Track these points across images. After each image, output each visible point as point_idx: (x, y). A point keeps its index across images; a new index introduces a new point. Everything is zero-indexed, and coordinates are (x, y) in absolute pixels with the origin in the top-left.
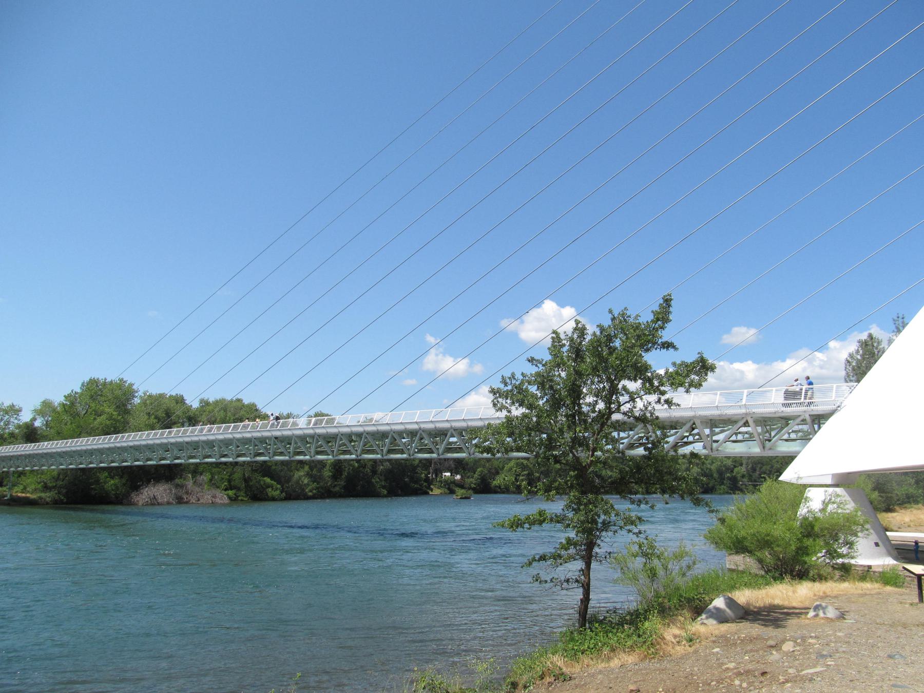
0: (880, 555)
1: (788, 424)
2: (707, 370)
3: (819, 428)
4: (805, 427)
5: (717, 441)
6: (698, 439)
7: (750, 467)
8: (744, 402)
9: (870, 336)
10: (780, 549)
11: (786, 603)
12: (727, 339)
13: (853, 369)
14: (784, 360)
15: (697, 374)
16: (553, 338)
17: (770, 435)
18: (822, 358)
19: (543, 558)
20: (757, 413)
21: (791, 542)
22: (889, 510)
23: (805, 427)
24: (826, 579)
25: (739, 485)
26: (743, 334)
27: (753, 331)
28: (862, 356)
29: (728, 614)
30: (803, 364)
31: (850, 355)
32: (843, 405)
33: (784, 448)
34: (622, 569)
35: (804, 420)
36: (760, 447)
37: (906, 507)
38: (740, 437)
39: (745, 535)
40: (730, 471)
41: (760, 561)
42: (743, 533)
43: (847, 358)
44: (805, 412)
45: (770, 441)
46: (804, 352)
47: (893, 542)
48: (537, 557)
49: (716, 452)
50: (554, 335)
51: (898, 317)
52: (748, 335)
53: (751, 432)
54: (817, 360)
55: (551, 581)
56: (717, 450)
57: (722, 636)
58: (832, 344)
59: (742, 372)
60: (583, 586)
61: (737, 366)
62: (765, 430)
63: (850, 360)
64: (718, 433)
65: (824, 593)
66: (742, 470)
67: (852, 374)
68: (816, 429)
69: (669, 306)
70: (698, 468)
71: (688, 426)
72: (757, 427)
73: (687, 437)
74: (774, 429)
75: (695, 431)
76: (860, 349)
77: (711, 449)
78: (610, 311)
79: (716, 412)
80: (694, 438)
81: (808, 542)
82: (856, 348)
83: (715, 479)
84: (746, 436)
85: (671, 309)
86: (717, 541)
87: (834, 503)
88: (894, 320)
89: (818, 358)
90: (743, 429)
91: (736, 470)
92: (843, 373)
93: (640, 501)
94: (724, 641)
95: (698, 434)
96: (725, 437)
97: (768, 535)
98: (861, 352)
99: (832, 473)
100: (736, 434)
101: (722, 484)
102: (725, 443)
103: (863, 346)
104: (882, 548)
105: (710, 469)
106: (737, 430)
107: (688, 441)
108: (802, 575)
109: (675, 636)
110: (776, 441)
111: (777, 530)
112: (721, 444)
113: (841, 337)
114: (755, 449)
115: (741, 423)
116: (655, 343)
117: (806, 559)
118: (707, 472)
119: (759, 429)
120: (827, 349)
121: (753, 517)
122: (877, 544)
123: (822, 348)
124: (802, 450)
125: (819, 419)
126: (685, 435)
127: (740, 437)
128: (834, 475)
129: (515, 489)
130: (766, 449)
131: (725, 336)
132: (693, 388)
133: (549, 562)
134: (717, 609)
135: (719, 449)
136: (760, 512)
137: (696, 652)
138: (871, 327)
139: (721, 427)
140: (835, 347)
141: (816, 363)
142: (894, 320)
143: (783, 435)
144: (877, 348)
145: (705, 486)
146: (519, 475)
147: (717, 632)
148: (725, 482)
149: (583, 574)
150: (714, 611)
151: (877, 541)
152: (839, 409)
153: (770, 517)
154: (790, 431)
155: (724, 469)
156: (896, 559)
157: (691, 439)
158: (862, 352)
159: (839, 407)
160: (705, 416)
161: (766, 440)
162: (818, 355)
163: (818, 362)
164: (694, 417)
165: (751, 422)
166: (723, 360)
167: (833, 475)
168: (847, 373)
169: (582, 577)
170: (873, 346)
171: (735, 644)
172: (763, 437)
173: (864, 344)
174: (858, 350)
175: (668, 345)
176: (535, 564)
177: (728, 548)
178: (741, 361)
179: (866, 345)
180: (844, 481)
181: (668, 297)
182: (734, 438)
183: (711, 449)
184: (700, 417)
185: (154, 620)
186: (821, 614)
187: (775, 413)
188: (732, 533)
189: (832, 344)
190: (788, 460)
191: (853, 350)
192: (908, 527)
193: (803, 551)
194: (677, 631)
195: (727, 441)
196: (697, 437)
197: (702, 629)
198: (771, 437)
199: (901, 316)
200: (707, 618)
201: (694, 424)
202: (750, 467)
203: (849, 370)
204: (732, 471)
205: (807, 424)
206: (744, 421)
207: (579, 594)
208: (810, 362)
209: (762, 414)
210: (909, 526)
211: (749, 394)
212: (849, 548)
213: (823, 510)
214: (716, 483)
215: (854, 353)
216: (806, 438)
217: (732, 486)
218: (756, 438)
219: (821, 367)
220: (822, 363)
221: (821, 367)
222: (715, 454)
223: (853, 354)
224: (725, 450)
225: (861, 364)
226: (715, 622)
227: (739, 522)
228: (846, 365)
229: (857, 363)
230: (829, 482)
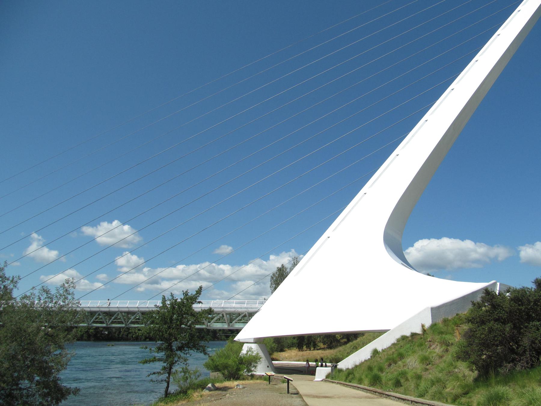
0: (269, 371)
10: (230, 369)
11: (230, 386)
12: (218, 251)
16: (163, 298)
19: (154, 373)
21: (234, 366)
22: (282, 350)
24: (245, 380)
25: (217, 336)
26: (226, 249)
28: (278, 275)
29: (474, 256)
32: (260, 309)
33: (237, 326)
34: (174, 378)
37: (291, 349)
39: (219, 364)
41: (223, 374)
42: (218, 363)
44: (246, 311)
47: (274, 366)
48: (152, 373)
50: (163, 297)
55: (156, 381)
56: (210, 326)
57: (210, 395)
58: (272, 257)
59: (223, 271)
60: (167, 382)
61: (222, 266)
65: (243, 383)
69: (201, 290)
76: (278, 272)
77: (207, 326)
78: (183, 291)
81: (241, 366)
82: (276, 271)
83: (205, 332)
86: (207, 366)
87: (251, 351)
93: (187, 353)
94: (211, 396)
97: (227, 364)
98: (278, 273)
101: (208, 334)
104: (270, 368)
108: (237, 379)
109: (197, 395)
111: (230, 362)
114: (225, 326)
116: (196, 301)
117: (239, 372)
121: (222, 357)
122: (268, 367)
129: (86, 338)
133: (156, 375)
134: (209, 387)
136: (224, 355)
137: (203, 399)
144: (285, 272)
146: (90, 329)
147: (209, 394)
148: (210, 334)
149: (167, 378)
150: (208, 388)
151: (269, 365)
153: (228, 357)
156: (274, 372)
159: (259, 310)
167: (254, 338)
168: (271, 283)
169: (167, 380)
170: (283, 271)
171: (214, 396)
175: (200, 302)
176: (151, 375)
177: (212, 369)
178: (225, 264)
179: (280, 270)
180: (259, 341)
183: (207, 326)
186: (238, 387)
187: (234, 311)
188: (214, 363)
189: (272, 257)
190: (238, 331)
192: (290, 359)
193: (238, 369)
194: (197, 394)
197: (205, 393)
200: (206, 390)
207: (165, 384)
209: (230, 311)
210: (287, 358)
212: (255, 368)
213: (247, 354)
214: (205, 334)
217: (213, 336)
222: (208, 328)
226: (208, 391)
227: (217, 359)
228: (271, 279)
230: (252, 341)
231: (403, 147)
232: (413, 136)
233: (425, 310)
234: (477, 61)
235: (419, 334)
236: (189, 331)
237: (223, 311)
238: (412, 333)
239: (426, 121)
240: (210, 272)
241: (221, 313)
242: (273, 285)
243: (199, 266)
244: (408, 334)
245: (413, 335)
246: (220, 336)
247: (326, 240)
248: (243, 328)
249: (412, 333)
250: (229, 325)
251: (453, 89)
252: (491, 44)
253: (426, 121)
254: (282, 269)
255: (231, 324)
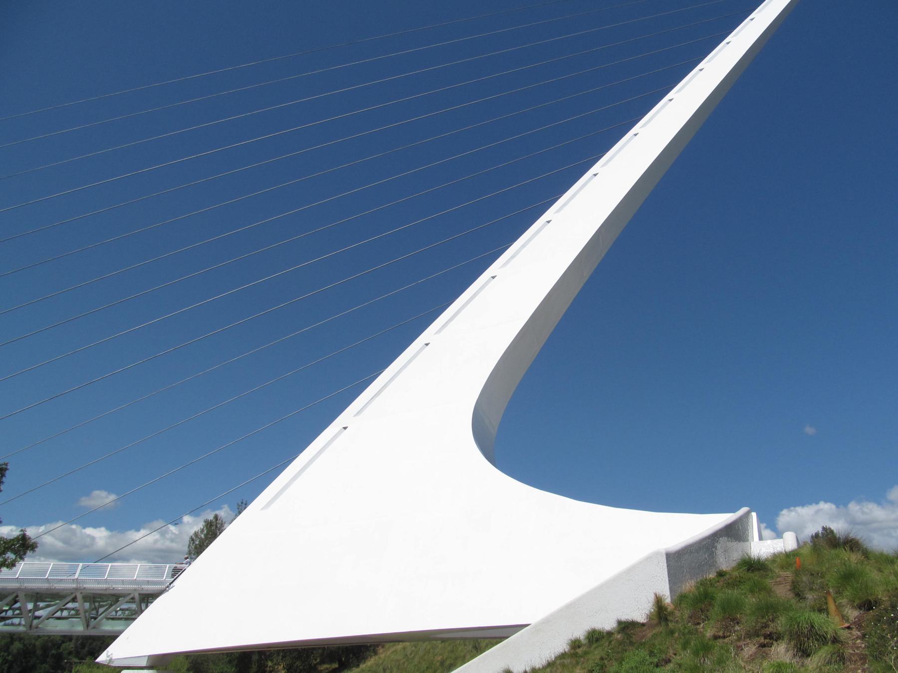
1: (117, 601)
2: (27, 549)
3: (147, 607)
4: (134, 606)
5: (39, 617)
6: (18, 614)
7: (79, 642)
8: (76, 576)
9: (216, 517)
12: (85, 502)
13: (196, 548)
14: (138, 530)
15: (16, 552)
17: (97, 612)
18: (174, 531)
20: (88, 589)
23: (134, 606)
25: (63, 664)
26: (103, 498)
27: (113, 497)
28: (206, 535)
30: (156, 536)
31: (195, 533)
33: (108, 627)
35: (133, 598)
36: (83, 624)
38: (65, 613)
40: (56, 647)
43: (192, 536)
44: (135, 590)
45: (95, 618)
46: (158, 524)
49: (35, 630)
51: (242, 503)
52: (107, 501)
53: (78, 608)
54: (170, 532)
56: (37, 627)
58: (187, 519)
59: (93, 538)
61: (89, 531)
62: (93, 606)
63: (195, 538)
64: (42, 608)
66: (71, 645)
67: (193, 552)
68: (143, 608)
70: (20, 643)
71: (10, 598)
72: (85, 603)
73: (6, 611)
74: (103, 606)
75: (17, 605)
76: (205, 528)
79: (45, 586)
80: (13, 613)
82: (202, 527)
84: (73, 612)
85: (4, 479)
88: (238, 505)
89: (171, 531)
90: (70, 605)
91: (64, 645)
92: (186, 549)
95: (19, 609)
96: (48, 614)
98: (205, 532)
99: (148, 655)
100: (62, 610)
102: (48, 619)
103: (208, 526)
105: (34, 645)
106: (64, 606)
107: (6, 616)
110: (102, 619)
112: (43, 621)
113: (194, 512)
114: (78, 628)
115: (70, 598)
118: (30, 648)
119: (87, 605)
120: (181, 522)
123: (177, 522)
124: (126, 629)
125: (148, 598)
126: (4, 608)
127: (65, 613)
128: (150, 657)
130: (89, 628)
131: (83, 499)
132: (5, 568)
135: (40, 626)
138: (224, 506)
139: (45, 602)
140: (188, 522)
141: (168, 536)
142: (238, 505)
143: (111, 613)
145: (24, 664)
148: (48, 660)
152: (168, 589)
154: (118, 609)
155: (50, 644)
157: (10, 613)
158: (207, 532)
159: (167, 587)
160: (31, 589)
161: (92, 618)
162: (172, 528)
163: (170, 535)
164: (19, 589)
165: (79, 597)
166: (76, 524)
167: (150, 656)
170: (216, 527)
172: (89, 614)
173: (209, 524)
174: (203, 529)
178: (96, 526)
181: (4, 466)
182: (58, 614)
184: (26, 590)
185: (876, 646)
187: (106, 589)
189: (187, 519)
190: (106, 641)
191: (199, 529)
195: (51, 618)
196: (17, 612)
198: (97, 615)
199: (245, 502)
201: (17, 596)
202: (79, 642)
203: (192, 548)
204: (59, 648)
205: (134, 602)
206: (73, 596)
208: (163, 535)
209: (66, 589)
211: (84, 568)
215: (199, 532)
216: (130, 617)
218: (82, 615)
219: (172, 541)
220: (173, 536)
221: (172, 541)
223: (198, 532)
224: (45, 628)
225: (203, 543)
228: (190, 543)
229: (200, 542)
230: (144, 663)
231: (708, 62)
232: (523, 246)
233: (649, 559)
234: (636, 135)
235: (643, 625)
236: (3, 655)
237: (76, 589)
238: (620, 623)
239: (548, 222)
240: (66, 541)
241: (72, 593)
242: (192, 554)
243: (42, 529)
244: (608, 624)
245: (626, 627)
246: (68, 665)
247: (421, 349)
248: (121, 632)
249: (620, 623)
250: (88, 626)
251: (595, 175)
252: (720, 50)
253: (548, 222)
254: (215, 524)
255: (93, 622)
